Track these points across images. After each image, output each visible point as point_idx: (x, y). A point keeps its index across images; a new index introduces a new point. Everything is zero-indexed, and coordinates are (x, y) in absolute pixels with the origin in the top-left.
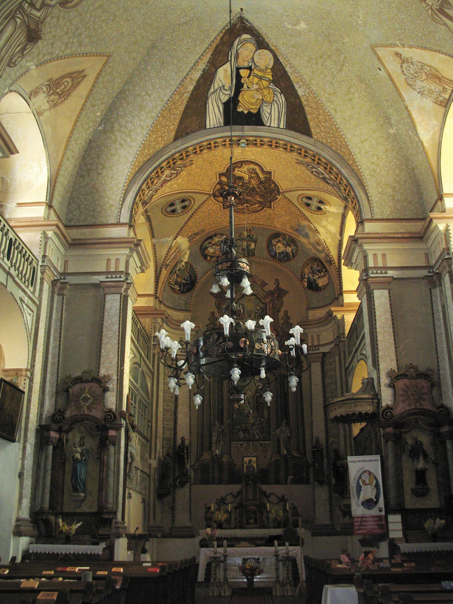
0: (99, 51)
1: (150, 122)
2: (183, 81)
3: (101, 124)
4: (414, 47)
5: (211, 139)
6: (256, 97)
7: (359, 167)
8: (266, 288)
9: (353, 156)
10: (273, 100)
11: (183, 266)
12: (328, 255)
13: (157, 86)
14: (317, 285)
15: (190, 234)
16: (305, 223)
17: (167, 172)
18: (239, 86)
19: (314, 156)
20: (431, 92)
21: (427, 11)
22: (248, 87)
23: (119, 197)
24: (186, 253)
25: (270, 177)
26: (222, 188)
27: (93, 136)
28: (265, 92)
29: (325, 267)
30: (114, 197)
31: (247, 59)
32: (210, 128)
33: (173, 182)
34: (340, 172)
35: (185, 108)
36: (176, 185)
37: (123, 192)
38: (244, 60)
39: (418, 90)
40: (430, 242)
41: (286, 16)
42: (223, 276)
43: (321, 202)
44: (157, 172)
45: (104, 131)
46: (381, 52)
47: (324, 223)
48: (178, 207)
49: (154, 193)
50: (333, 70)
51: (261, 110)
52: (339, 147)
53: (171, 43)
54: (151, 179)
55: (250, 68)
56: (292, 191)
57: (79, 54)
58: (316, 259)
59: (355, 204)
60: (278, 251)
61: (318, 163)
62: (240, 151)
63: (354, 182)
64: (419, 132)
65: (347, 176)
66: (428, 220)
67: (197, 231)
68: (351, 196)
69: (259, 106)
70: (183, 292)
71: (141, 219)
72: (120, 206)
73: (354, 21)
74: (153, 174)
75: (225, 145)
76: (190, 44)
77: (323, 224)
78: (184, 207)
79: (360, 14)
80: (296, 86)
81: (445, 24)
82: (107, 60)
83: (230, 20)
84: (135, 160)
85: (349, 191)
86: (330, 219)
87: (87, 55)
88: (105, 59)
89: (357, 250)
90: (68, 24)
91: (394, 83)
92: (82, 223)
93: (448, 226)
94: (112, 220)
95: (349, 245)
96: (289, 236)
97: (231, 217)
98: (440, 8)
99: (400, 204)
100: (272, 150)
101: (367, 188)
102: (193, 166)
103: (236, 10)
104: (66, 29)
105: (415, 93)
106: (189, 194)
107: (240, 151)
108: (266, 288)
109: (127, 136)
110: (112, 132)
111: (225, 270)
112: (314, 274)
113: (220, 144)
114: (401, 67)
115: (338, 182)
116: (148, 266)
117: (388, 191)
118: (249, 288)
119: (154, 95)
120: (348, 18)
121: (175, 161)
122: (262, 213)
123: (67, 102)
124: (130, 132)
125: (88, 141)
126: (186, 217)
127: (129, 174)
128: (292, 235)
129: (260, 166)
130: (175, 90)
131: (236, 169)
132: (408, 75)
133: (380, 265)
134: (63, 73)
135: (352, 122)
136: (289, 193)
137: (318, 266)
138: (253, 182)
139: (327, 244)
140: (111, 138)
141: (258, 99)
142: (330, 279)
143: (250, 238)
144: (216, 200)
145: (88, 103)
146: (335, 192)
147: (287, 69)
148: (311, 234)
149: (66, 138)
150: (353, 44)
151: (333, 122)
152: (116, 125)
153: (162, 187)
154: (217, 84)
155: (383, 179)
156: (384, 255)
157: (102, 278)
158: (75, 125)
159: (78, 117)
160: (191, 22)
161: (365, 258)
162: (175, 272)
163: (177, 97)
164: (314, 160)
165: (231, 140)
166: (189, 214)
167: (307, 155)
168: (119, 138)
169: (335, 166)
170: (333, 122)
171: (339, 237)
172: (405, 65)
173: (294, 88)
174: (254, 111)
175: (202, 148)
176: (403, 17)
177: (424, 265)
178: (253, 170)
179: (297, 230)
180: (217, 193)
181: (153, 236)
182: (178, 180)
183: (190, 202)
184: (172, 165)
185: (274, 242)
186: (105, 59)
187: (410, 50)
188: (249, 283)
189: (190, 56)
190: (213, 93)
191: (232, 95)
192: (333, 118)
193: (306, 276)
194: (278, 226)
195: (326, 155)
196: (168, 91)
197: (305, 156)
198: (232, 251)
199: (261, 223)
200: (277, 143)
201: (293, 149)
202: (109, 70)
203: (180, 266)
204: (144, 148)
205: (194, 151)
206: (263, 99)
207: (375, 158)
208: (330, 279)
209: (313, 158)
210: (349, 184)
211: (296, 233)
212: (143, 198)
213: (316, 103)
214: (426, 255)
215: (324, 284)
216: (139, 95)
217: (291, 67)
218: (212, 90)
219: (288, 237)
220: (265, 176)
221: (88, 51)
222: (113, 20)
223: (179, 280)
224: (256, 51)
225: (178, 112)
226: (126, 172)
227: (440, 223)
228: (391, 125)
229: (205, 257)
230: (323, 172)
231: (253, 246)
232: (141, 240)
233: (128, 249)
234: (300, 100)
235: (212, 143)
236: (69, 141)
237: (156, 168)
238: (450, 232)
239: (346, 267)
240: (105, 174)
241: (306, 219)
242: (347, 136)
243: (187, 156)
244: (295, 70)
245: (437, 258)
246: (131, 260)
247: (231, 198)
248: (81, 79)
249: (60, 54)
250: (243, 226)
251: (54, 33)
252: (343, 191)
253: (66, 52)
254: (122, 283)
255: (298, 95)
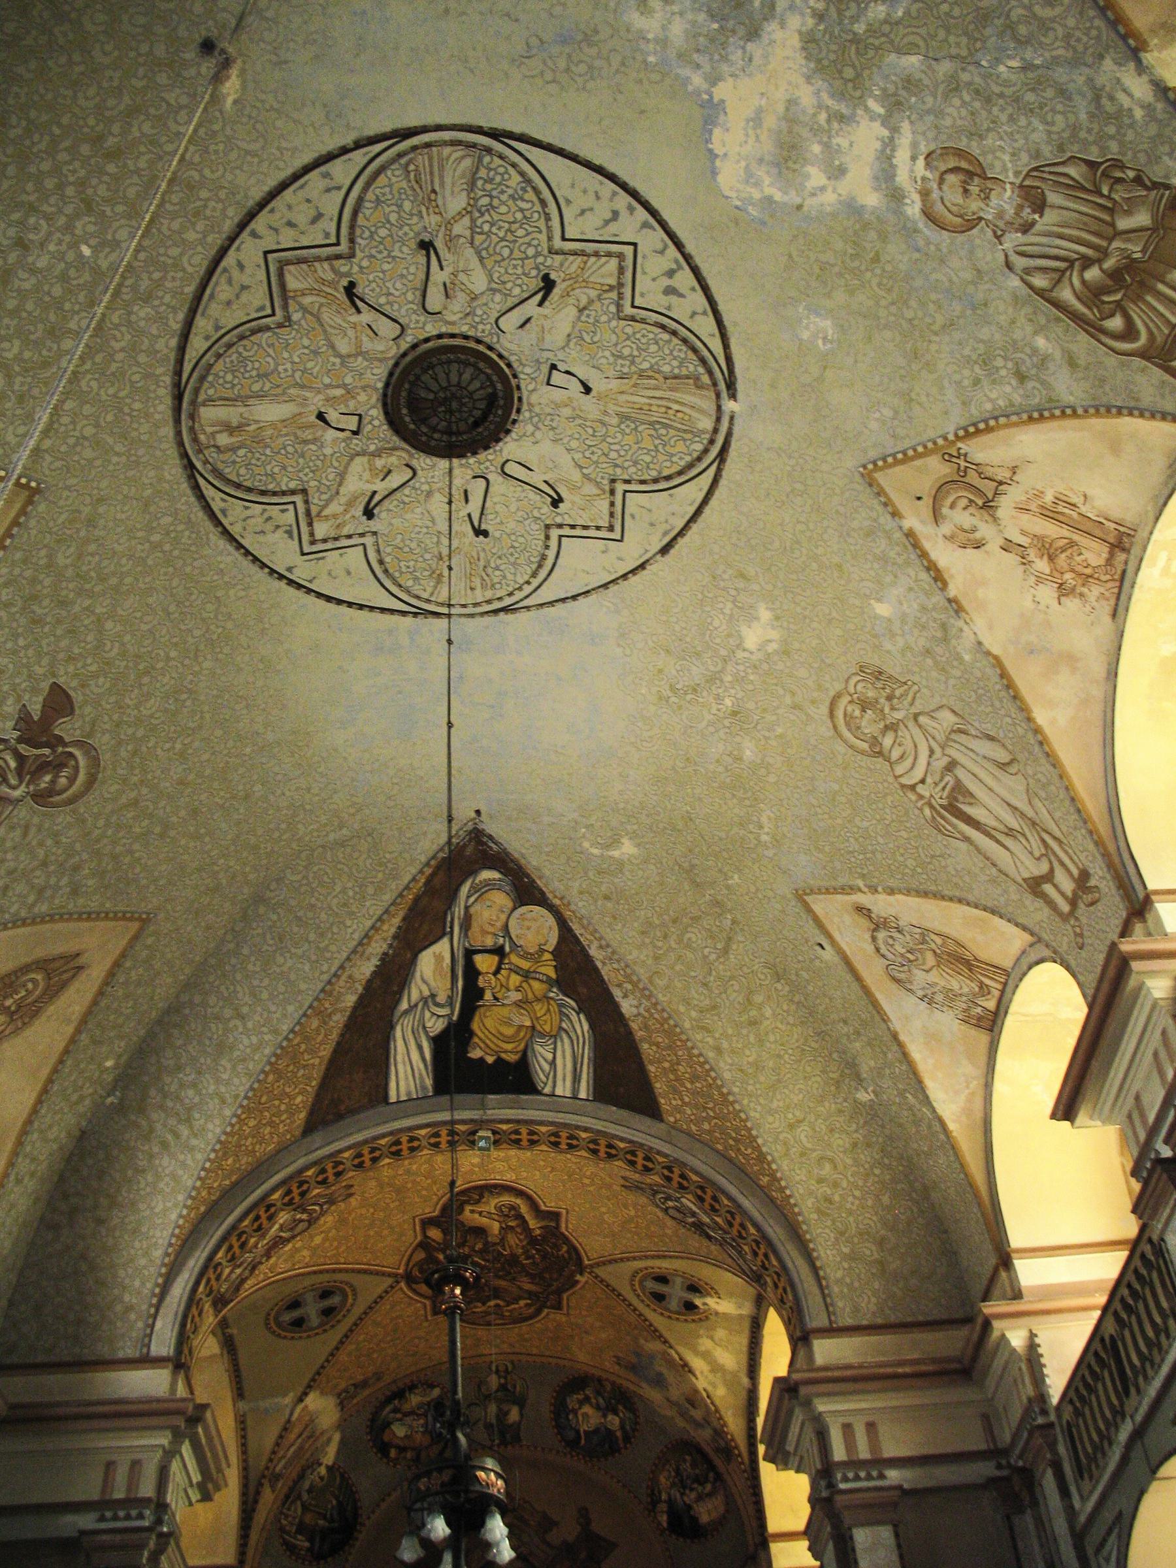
0: (121, 908)
1: (241, 1085)
2: (329, 982)
3: (114, 1089)
4: (900, 892)
5: (401, 1131)
6: (517, 1021)
7: (788, 1192)
8: (555, 1537)
9: (769, 1164)
10: (561, 1028)
11: (322, 1478)
12: (719, 1433)
13: (265, 996)
14: (694, 1520)
15: (343, 1385)
16: (653, 1346)
17: (283, 1217)
18: (472, 996)
19: (670, 1169)
20: (951, 996)
21: (921, 809)
22: (496, 999)
23: (149, 1285)
24: (329, 1440)
25: (558, 1227)
26: (431, 1259)
27: (90, 1121)
28: (540, 1009)
29: (712, 1467)
30: (137, 1283)
31: (491, 929)
32: (398, 1102)
33: (299, 1245)
34: (739, 1206)
35: (335, 1051)
36: (305, 1253)
37: (164, 1270)
38: (484, 932)
39: (920, 993)
40: (991, 1382)
41: (587, 827)
42: (431, 1511)
43: (694, 1288)
44: (258, 1218)
45: (121, 1109)
46: (819, 905)
47: (705, 1344)
48: (312, 1310)
49: (247, 1273)
50: (706, 951)
51: (529, 1054)
52: (731, 1142)
53: (303, 889)
54: (240, 1236)
55: (499, 951)
56: (615, 1261)
57: (71, 914)
58: (688, 1447)
59: (785, 1290)
60: (584, 1427)
61: (681, 1187)
62: (476, 1160)
63: (775, 1232)
64: (932, 1096)
65: (756, 1215)
66: (980, 1320)
67: (360, 1378)
68: (772, 1270)
69: (522, 1046)
70: (319, 1557)
71: (208, 1346)
72: (152, 1310)
73: (751, 836)
74: (246, 1223)
75: (436, 1145)
76: (351, 893)
77: (702, 1348)
78: (328, 1312)
79: (764, 820)
80: (617, 993)
81: (967, 839)
82: (141, 930)
83: (450, 837)
84: (198, 1183)
85: (766, 1255)
86: (721, 1333)
87: (89, 916)
88: (134, 926)
89: (799, 1416)
90: (49, 842)
91: (858, 978)
92: (40, 1359)
93: (1032, 1336)
94: (129, 1351)
95: (774, 1403)
96: (613, 1383)
97: (453, 1342)
98: (951, 805)
99: (901, 1285)
100: (561, 1157)
101: (811, 1246)
102: (353, 1201)
103: (464, 812)
104: (41, 853)
105: (913, 1000)
106: (339, 1277)
107: (476, 1160)
108: (555, 1537)
109: (180, 1121)
110: (142, 1111)
111: (437, 1494)
112: (684, 1487)
113: (424, 1143)
114: (874, 939)
115: (735, 1232)
116: (222, 1483)
117: (868, 1252)
118: (506, 1544)
119: (257, 1018)
120: (735, 829)
121: (305, 1187)
122: (538, 1324)
123: (28, 1032)
124: (189, 1110)
125: (77, 1133)
126: (334, 1336)
127: (181, 1222)
128: (619, 1381)
129: (529, 1199)
130: (310, 1007)
131: (468, 1208)
132: (890, 956)
133: (864, 1453)
134: (28, 960)
135: (762, 1079)
136: (610, 1268)
137: (694, 1465)
138: (512, 1239)
139: (717, 1402)
140: (138, 1126)
141: (521, 1027)
142: (729, 1499)
143: (507, 1394)
144: (415, 1291)
145: (83, 1036)
146: (729, 1261)
147: (593, 952)
148: (670, 1377)
149: (19, 1124)
150: (753, 889)
151: (714, 1079)
152: (152, 1092)
153: (269, 1257)
154: (415, 991)
155: (851, 1219)
156: (871, 1426)
157: (87, 1521)
158: (45, 1091)
159: (55, 1070)
160: (355, 840)
161: (822, 1436)
162: (299, 1497)
163: (315, 1023)
164: (669, 1179)
165: (452, 1133)
166: (343, 1328)
167: (650, 1165)
168: (158, 1126)
169: (724, 1192)
170: (714, 1079)
171: (745, 1381)
172: (881, 935)
173: (610, 996)
174: (512, 1058)
175: (377, 1154)
176: (865, 824)
177: (983, 1446)
178: (512, 1208)
179: (633, 1368)
180: (416, 1272)
181: (239, 1393)
182: (312, 1237)
183: (345, 1296)
184: (297, 1199)
185: (572, 1401)
186: (134, 926)
187: (891, 899)
188: (505, 1531)
189: (349, 923)
190: (406, 1012)
191: (455, 1018)
192: (712, 1069)
193: (664, 1497)
194: (582, 1358)
195: (700, 1163)
196: (290, 1009)
197: (647, 1169)
198: (455, 1440)
199: (535, 1351)
200: (571, 1137)
201: (613, 1152)
202: (145, 953)
203: (312, 1478)
204: (225, 1154)
205: (356, 1161)
206: (533, 1027)
207: (828, 1167)
208: (729, 1499)
209: (666, 1172)
210: (765, 1237)
211: (631, 1377)
212: (215, 1287)
213: (669, 1033)
214: (985, 1417)
215: (714, 1515)
216: (217, 1018)
217: (601, 947)
218: (404, 1005)
219: (609, 1387)
220: (543, 1223)
221: (94, 905)
222: (162, 836)
223: (308, 1519)
224: (515, 908)
225: (317, 1061)
226: (174, 1216)
227: (1013, 1328)
228: (859, 1079)
229: (383, 1449)
230: (694, 1208)
231: (514, 1415)
232: (204, 1407)
233: (168, 1433)
234: (626, 1026)
235: (404, 1139)
236: (24, 1132)
237: (255, 1205)
238: (1040, 1350)
239: (772, 1466)
240: (116, 1221)
241: (656, 1334)
242: (752, 1114)
243: (338, 1174)
244: (614, 952)
245: (1014, 1424)
246: (175, 1466)
247: (453, 1290)
248: (70, 974)
249: (23, 914)
250: (487, 1359)
251: (12, 864)
252: (749, 1257)
253: (36, 910)
254: (144, 1535)
255: (621, 1015)
